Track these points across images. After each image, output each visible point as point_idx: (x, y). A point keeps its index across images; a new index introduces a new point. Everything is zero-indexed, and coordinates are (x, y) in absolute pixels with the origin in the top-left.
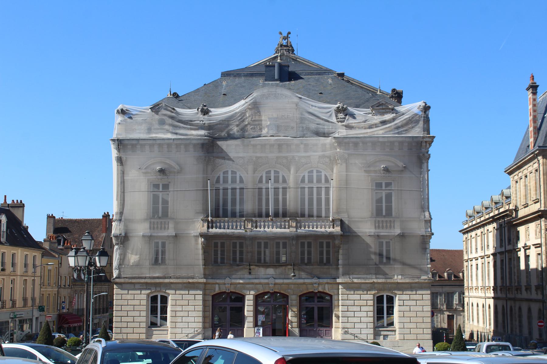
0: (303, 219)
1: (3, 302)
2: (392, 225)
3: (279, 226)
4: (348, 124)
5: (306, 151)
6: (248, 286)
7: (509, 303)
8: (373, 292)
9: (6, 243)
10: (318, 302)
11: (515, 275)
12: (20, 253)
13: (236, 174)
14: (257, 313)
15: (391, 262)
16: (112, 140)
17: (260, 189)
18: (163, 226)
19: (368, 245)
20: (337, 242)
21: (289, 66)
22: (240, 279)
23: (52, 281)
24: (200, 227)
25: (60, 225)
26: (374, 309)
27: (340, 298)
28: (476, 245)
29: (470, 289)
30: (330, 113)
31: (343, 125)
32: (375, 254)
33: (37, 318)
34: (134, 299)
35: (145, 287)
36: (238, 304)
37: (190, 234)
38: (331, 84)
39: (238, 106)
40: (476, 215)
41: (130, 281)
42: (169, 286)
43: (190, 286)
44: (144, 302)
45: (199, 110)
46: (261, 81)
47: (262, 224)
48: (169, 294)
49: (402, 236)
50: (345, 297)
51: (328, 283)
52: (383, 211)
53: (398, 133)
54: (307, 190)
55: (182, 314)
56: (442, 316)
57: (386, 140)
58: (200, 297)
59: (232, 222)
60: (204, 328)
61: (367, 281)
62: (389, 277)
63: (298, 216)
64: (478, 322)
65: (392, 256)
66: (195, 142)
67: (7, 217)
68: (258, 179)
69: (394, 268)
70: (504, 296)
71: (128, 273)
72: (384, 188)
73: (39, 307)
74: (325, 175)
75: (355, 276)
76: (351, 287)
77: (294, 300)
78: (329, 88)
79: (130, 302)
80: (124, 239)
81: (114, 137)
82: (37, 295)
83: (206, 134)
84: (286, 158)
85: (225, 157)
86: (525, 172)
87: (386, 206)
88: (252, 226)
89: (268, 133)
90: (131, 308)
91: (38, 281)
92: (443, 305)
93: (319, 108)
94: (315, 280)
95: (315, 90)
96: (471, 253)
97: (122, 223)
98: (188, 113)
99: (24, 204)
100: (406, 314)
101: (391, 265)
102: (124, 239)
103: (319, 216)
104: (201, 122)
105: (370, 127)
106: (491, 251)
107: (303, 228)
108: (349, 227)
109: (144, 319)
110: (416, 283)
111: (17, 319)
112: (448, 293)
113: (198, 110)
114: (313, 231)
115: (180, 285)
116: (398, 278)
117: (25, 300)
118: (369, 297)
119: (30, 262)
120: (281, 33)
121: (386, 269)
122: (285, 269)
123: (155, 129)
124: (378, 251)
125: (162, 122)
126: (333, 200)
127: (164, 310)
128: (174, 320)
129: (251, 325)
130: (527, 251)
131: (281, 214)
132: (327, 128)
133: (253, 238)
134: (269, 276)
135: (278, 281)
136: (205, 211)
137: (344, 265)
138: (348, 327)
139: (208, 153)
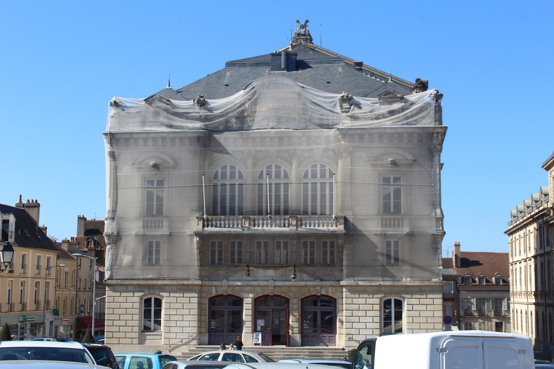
0: (306, 216)
1: (11, 305)
2: (401, 223)
3: (278, 224)
4: (354, 114)
5: (308, 144)
6: (246, 288)
8: (380, 296)
9: (14, 244)
10: (322, 306)
12: (31, 254)
13: (235, 169)
15: (400, 263)
16: (104, 134)
17: (261, 185)
18: (157, 225)
19: (374, 245)
20: (340, 241)
21: (297, 55)
22: (238, 281)
23: (69, 284)
24: (195, 226)
25: (91, 227)
26: (380, 314)
27: (344, 302)
28: (520, 248)
29: (515, 294)
30: (334, 103)
31: (348, 116)
32: (382, 254)
33: (51, 322)
35: (138, 289)
36: (236, 308)
37: (185, 232)
38: (340, 73)
39: (238, 97)
40: (520, 215)
41: (123, 283)
42: (163, 288)
43: (185, 289)
44: (137, 305)
45: (196, 101)
46: (267, 70)
47: (261, 222)
48: (163, 297)
49: (411, 235)
51: (331, 286)
52: (391, 208)
53: (407, 124)
54: (310, 186)
55: (176, 318)
56: (489, 323)
57: (394, 131)
58: (195, 300)
59: (233, 220)
60: (200, 333)
61: (373, 284)
62: (398, 279)
63: (300, 214)
64: (522, 330)
65: (400, 257)
66: (190, 135)
67: (16, 216)
68: (258, 174)
69: (403, 269)
70: (544, 302)
72: (392, 183)
73: (54, 310)
75: (360, 278)
76: (355, 290)
77: (295, 304)
78: (338, 76)
79: (123, 305)
80: (117, 238)
81: (107, 130)
82: (52, 298)
83: (203, 127)
84: (288, 151)
85: (222, 150)
87: (394, 202)
88: (250, 225)
89: (268, 125)
90: (124, 311)
91: (52, 283)
92: (490, 312)
93: (324, 97)
94: (317, 283)
95: (323, 80)
96: (516, 255)
98: (184, 104)
99: (39, 204)
100: (415, 320)
101: (400, 266)
102: (117, 238)
104: (197, 115)
105: (377, 118)
106: (532, 253)
107: (303, 227)
108: (353, 224)
109: (137, 323)
110: (426, 286)
111: (27, 323)
112: (496, 299)
113: (194, 101)
116: (407, 281)
117: (37, 302)
118: (375, 301)
119: (43, 264)
120: (298, 22)
121: (393, 270)
123: (149, 122)
124: (385, 252)
125: (156, 114)
127: (158, 313)
128: (168, 324)
129: (250, 330)
131: (282, 212)
132: (331, 118)
133: (253, 237)
134: (268, 278)
135: (277, 283)
136: (201, 209)
138: (352, 333)
139: (205, 147)
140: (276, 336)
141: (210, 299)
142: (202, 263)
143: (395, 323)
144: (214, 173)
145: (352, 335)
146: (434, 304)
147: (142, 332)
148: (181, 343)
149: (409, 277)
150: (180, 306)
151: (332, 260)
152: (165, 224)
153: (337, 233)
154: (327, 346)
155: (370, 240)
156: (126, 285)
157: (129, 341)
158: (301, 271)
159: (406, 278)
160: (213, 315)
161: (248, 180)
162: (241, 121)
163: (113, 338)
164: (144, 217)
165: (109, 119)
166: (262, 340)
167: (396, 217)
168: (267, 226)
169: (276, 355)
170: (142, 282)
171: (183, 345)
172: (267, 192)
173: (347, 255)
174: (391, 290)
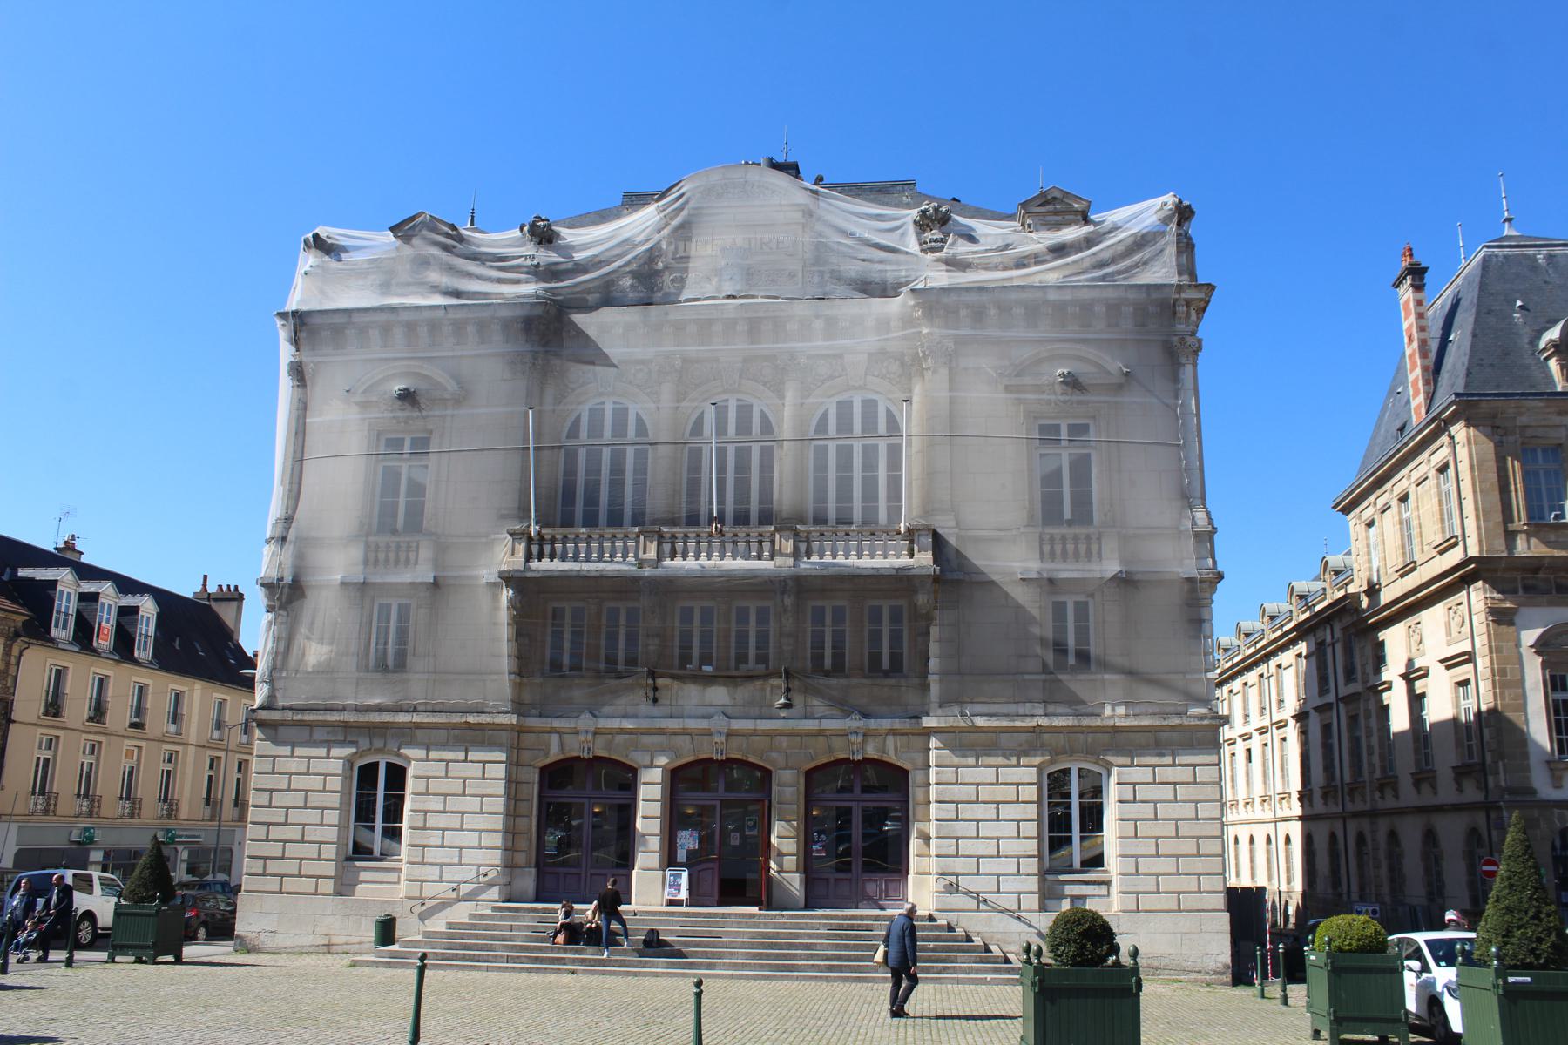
2: (1095, 548)
6: (647, 740)
7: (1352, 827)
8: (1037, 760)
11: (1370, 754)
14: (674, 820)
15: (1093, 667)
20: (922, 599)
24: (506, 556)
27: (933, 780)
31: (939, 260)
32: (1043, 641)
34: (308, 774)
39: (642, 223)
42: (409, 734)
43: (470, 737)
44: (335, 783)
48: (408, 760)
49: (1126, 582)
50: (949, 774)
51: (894, 732)
52: (1063, 508)
58: (499, 771)
60: (509, 865)
61: (1018, 724)
62: (1089, 710)
65: (1094, 649)
69: (1103, 681)
71: (295, 694)
74: (888, 411)
75: (979, 708)
76: (968, 744)
77: (787, 787)
79: (298, 782)
81: (292, 305)
83: (540, 293)
85: (592, 354)
86: (1398, 490)
89: (718, 290)
97: (289, 549)
99: (241, 595)
103: (869, 520)
104: (529, 262)
105: (1021, 263)
106: (1292, 705)
109: (331, 834)
110: (1173, 728)
111: (180, 848)
114: (834, 565)
115: (443, 733)
116: (1116, 715)
118: (1025, 774)
122: (763, 690)
124: (1049, 634)
125: (424, 262)
126: (909, 484)
127: (394, 811)
129: (655, 860)
130: (1418, 684)
131: (752, 518)
132: (892, 271)
133: (669, 589)
134: (711, 710)
135: (737, 725)
136: (523, 513)
137: (944, 673)
140: (732, 878)
141: (543, 770)
142: (524, 664)
143: (1082, 839)
144: (568, 424)
145: (957, 875)
146: (1195, 783)
147: (348, 859)
148: (454, 895)
149: (1120, 704)
150: (456, 786)
151: (896, 660)
152: (425, 553)
153: (913, 572)
154: (882, 908)
155: (1007, 595)
156: (310, 725)
157: (308, 884)
158: (808, 691)
159: (1113, 706)
160: (552, 814)
161: (661, 431)
162: (649, 282)
163: (264, 874)
164: (367, 535)
165: (299, 281)
166: (690, 889)
167: (1078, 530)
168: (709, 557)
169: (728, 934)
170: (350, 717)
171: (459, 900)
172: (711, 503)
173: (940, 641)
174: (1071, 741)
